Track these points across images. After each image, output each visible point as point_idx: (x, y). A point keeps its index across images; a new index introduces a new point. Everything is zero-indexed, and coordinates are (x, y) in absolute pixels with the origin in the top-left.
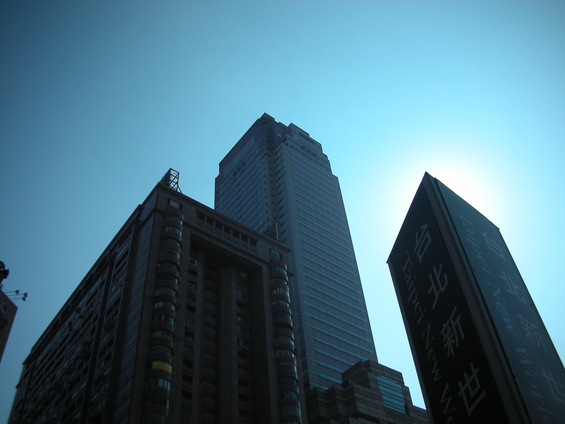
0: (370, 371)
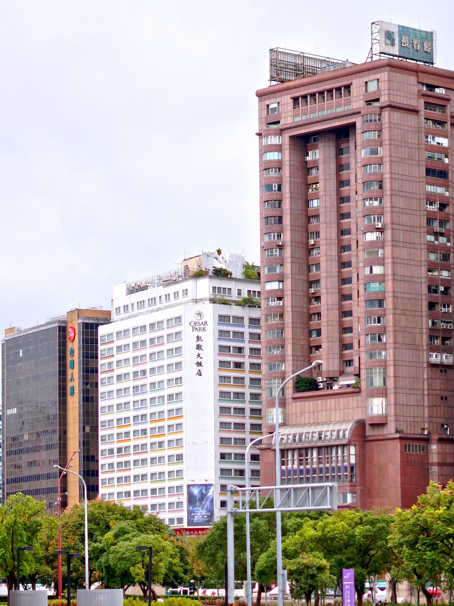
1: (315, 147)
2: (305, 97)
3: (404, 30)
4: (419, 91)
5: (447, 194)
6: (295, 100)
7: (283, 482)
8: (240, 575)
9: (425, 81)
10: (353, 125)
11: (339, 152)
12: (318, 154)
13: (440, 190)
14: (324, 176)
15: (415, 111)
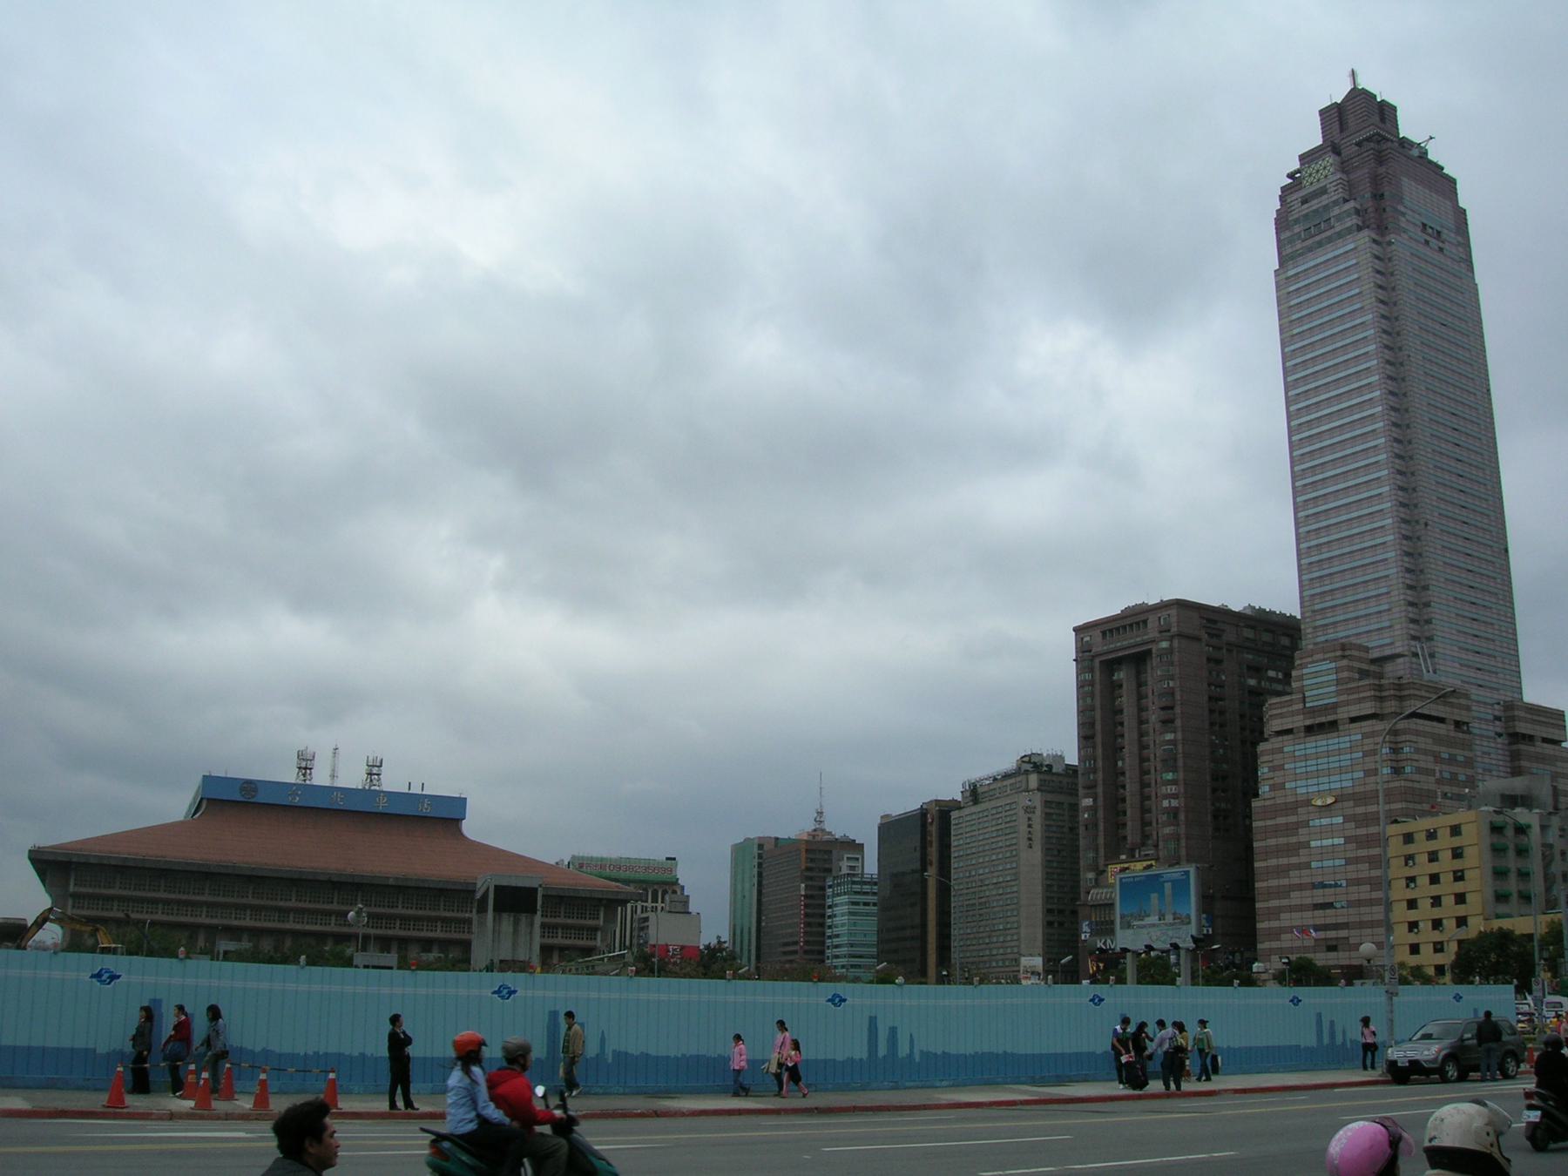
2: (1111, 631)
6: (1104, 633)
8: (454, 954)
10: (1149, 652)
11: (1138, 673)
12: (1120, 675)
15: (1198, 639)
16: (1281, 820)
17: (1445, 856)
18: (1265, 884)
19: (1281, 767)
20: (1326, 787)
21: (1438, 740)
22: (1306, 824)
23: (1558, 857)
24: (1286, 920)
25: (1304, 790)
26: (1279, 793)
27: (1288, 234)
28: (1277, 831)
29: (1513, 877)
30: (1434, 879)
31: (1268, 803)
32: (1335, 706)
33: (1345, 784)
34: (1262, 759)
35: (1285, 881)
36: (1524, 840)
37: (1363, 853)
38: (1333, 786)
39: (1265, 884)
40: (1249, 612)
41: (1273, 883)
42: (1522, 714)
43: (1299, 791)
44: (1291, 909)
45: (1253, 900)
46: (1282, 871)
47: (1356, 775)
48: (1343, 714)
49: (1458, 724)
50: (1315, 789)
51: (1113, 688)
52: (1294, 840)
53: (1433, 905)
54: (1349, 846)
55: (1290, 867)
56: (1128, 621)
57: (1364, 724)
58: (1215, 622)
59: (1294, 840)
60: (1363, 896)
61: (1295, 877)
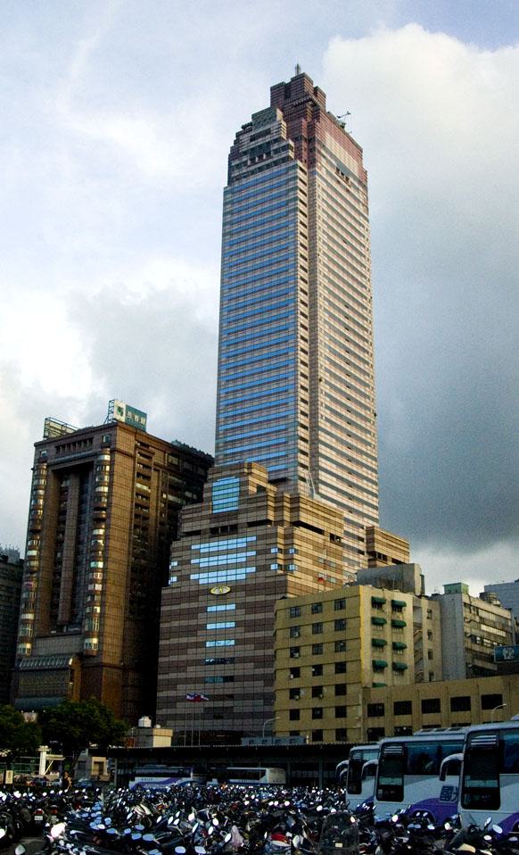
0: (250, 474)
1: (66, 479)
3: (128, 408)
4: (136, 445)
5: (149, 491)
6: (58, 448)
7: (197, 744)
9: (141, 440)
13: (145, 488)
14: (73, 493)
16: (184, 606)
17: (329, 627)
18: (166, 659)
19: (188, 562)
20: (224, 579)
21: (317, 547)
22: (204, 610)
23: (425, 636)
24: (181, 690)
25: (205, 581)
26: (184, 583)
27: (237, 162)
28: (180, 615)
29: (388, 649)
30: (317, 649)
31: (175, 591)
32: (237, 513)
33: (239, 577)
34: (174, 554)
35: (183, 658)
36: (398, 616)
37: (249, 635)
38: (229, 578)
39: (166, 659)
40: (175, 444)
41: (174, 658)
42: (380, 538)
43: (201, 582)
44: (186, 681)
45: (156, 674)
46: (183, 649)
47: (249, 554)
48: (243, 519)
49: (332, 537)
50: (215, 580)
51: (62, 493)
52: (193, 622)
53: (314, 674)
54: (239, 630)
55: (188, 646)
56: (79, 439)
57: (259, 528)
58: (148, 446)
59: (193, 622)
60: (248, 672)
61: (192, 654)
